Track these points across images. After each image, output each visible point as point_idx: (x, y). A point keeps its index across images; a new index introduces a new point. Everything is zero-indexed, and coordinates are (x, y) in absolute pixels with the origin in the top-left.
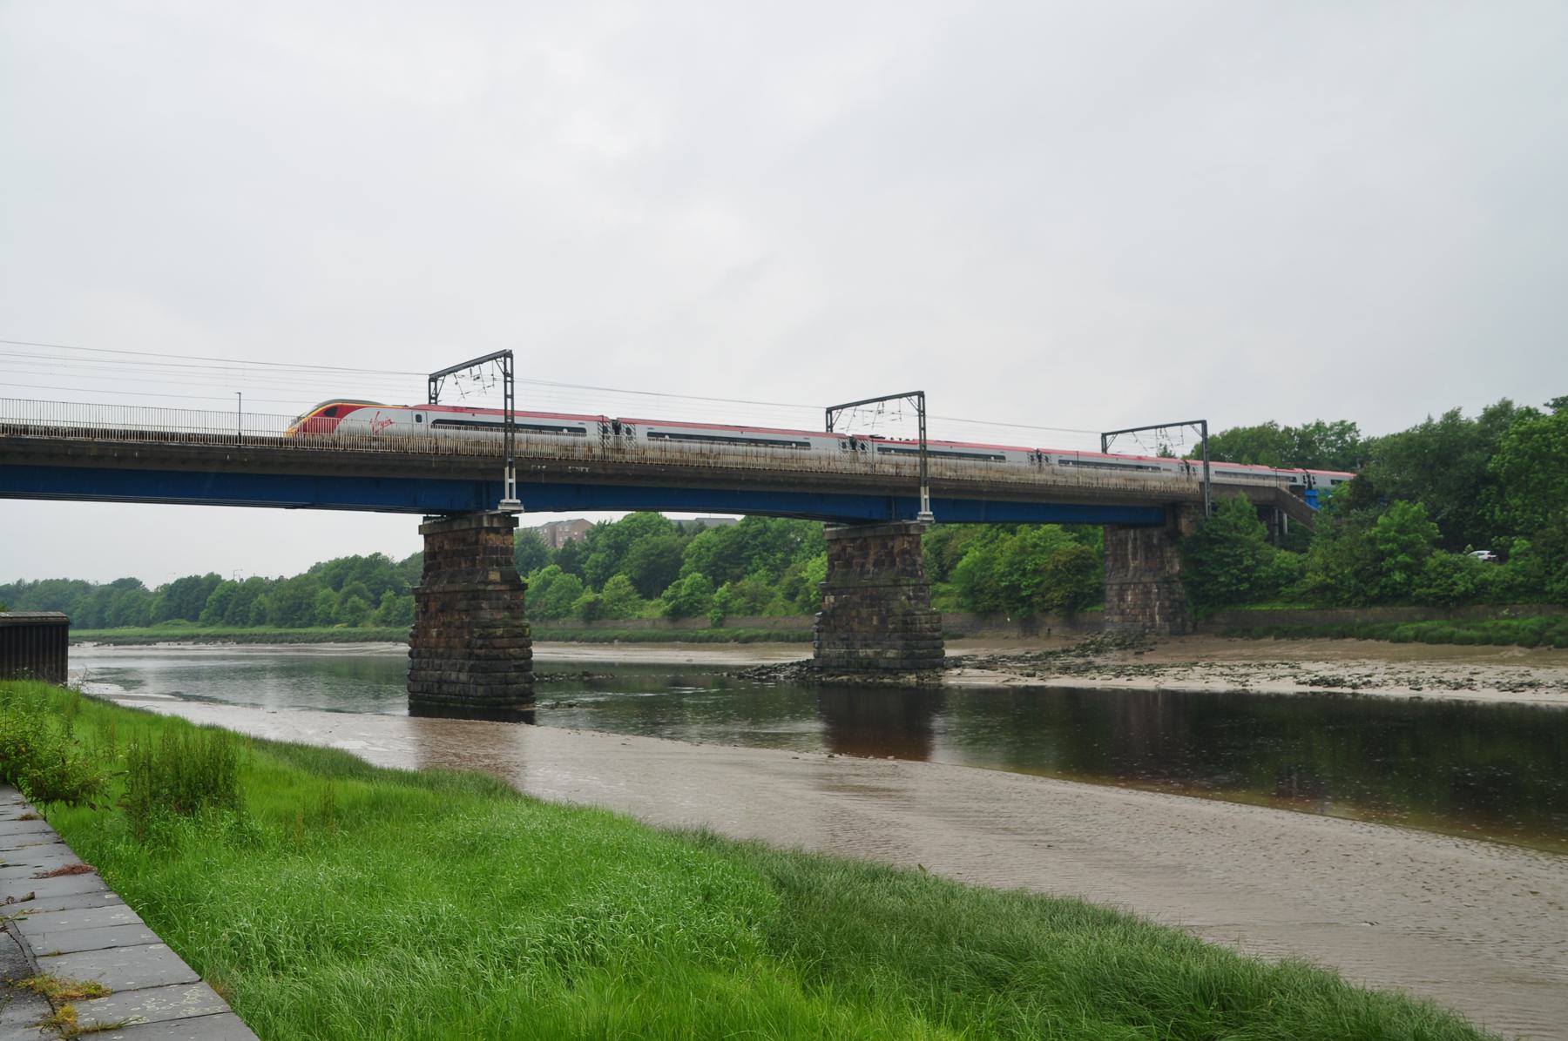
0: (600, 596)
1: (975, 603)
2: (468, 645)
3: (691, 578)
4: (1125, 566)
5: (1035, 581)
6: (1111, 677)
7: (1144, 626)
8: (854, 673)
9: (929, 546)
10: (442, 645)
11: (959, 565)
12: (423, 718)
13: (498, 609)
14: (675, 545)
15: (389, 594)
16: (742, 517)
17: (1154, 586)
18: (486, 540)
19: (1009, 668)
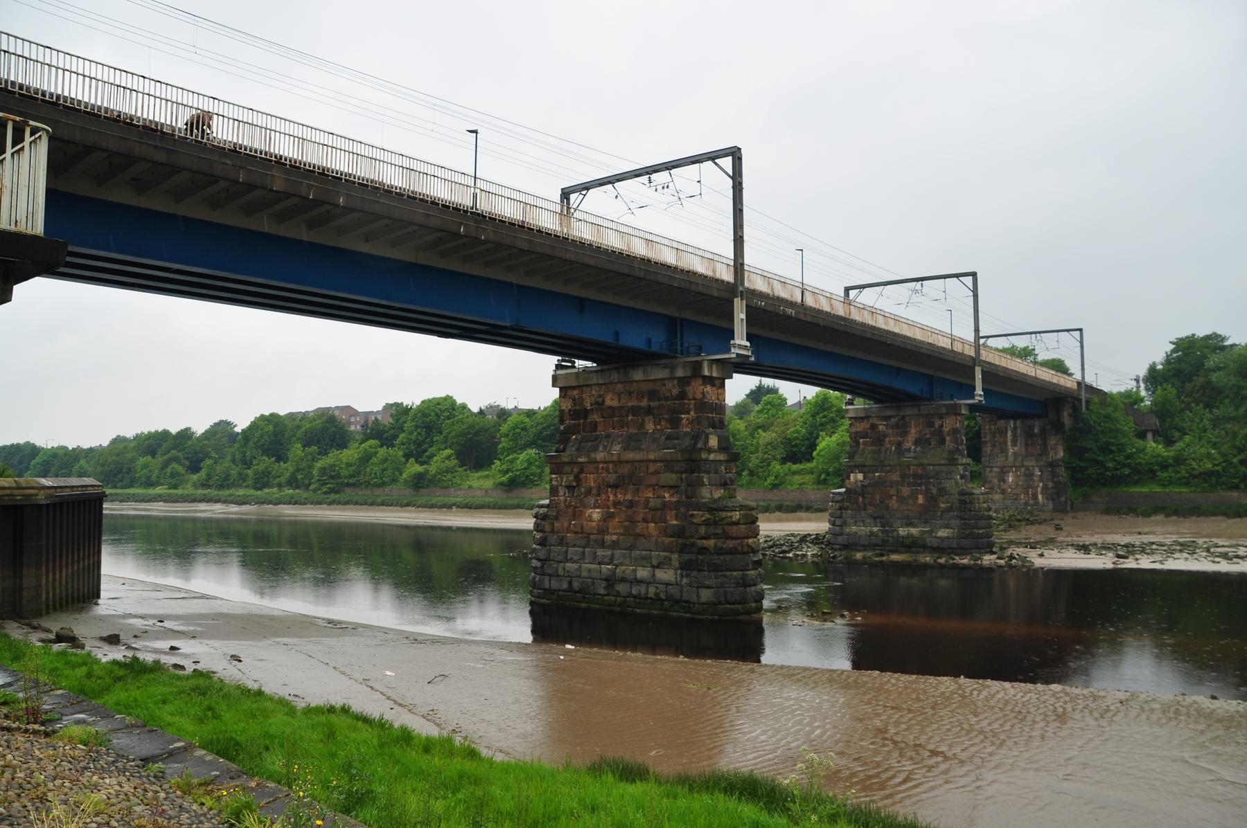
3: (527, 454)
4: (1004, 451)
16: (810, 392)
18: (703, 393)
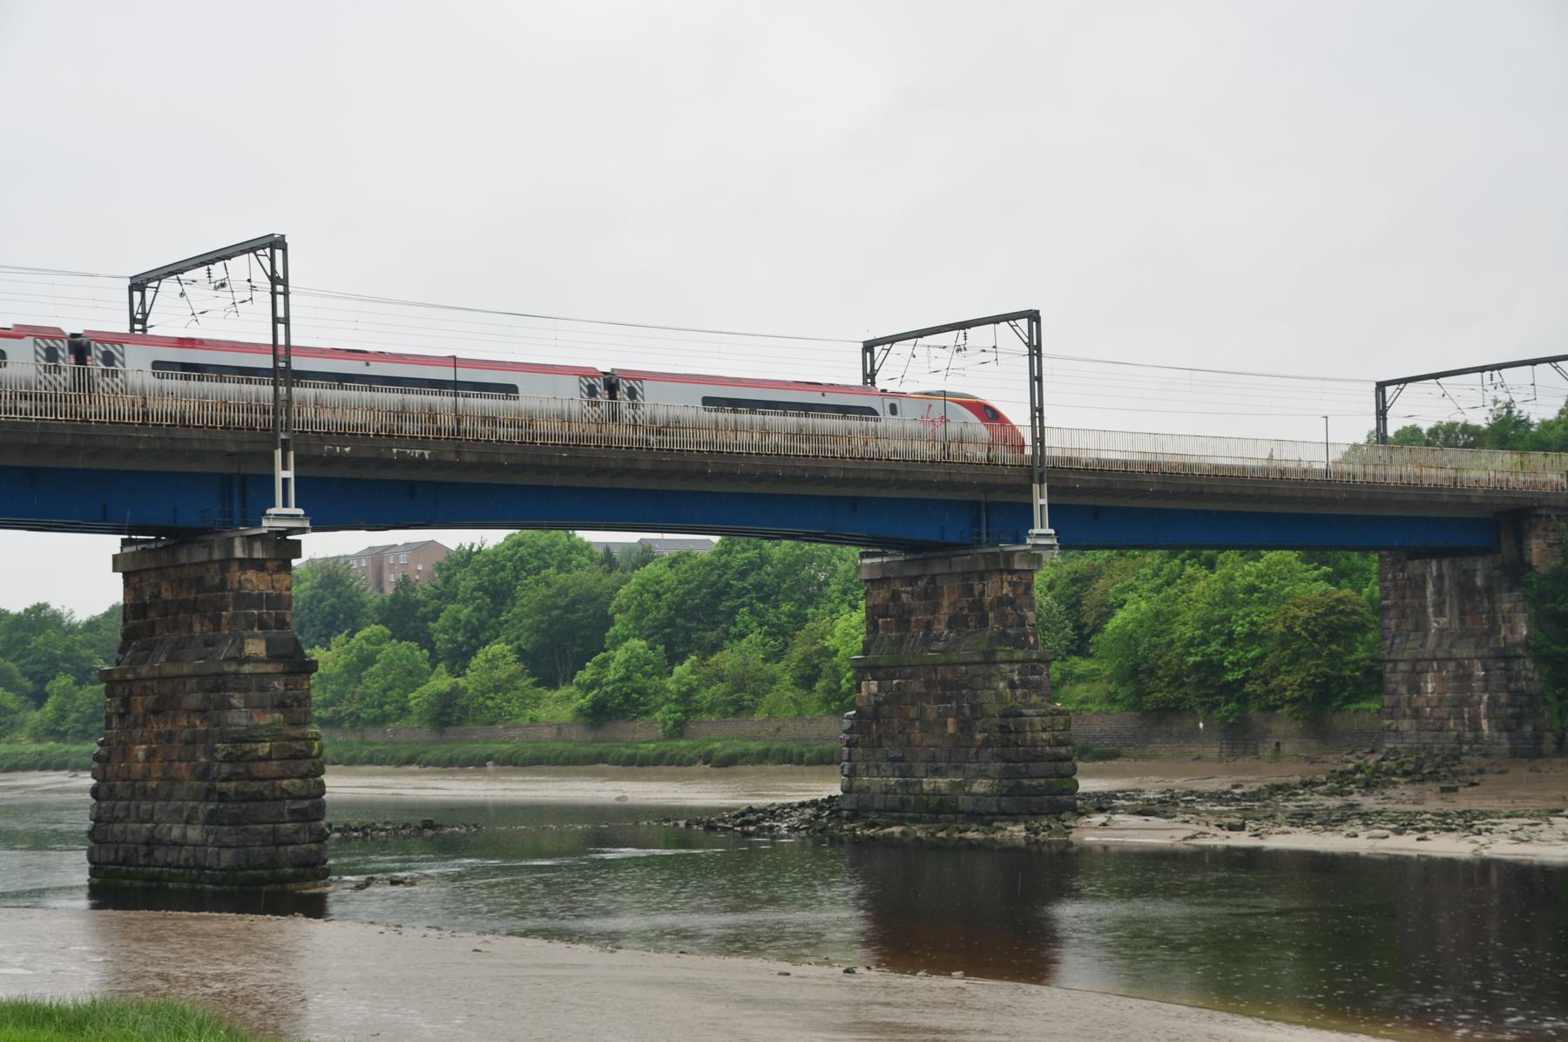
0: (461, 682)
1: (1140, 693)
2: (204, 775)
3: (627, 649)
4: (1421, 627)
5: (1250, 655)
6: (1386, 832)
7: (1459, 739)
8: (914, 821)
9: (1057, 590)
10: (155, 775)
11: (1111, 626)
12: (110, 912)
13: (263, 707)
14: (599, 589)
15: (64, 681)
17: (1478, 664)
18: (240, 582)
19: (1198, 813)
